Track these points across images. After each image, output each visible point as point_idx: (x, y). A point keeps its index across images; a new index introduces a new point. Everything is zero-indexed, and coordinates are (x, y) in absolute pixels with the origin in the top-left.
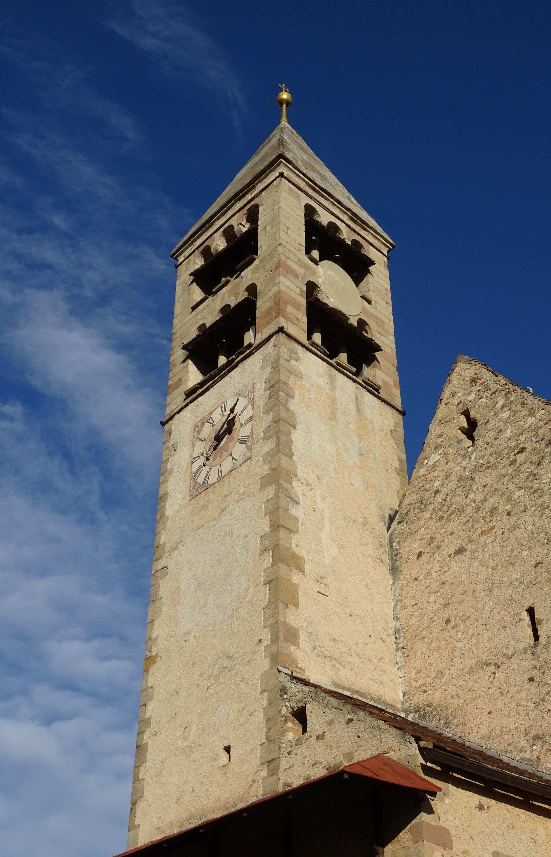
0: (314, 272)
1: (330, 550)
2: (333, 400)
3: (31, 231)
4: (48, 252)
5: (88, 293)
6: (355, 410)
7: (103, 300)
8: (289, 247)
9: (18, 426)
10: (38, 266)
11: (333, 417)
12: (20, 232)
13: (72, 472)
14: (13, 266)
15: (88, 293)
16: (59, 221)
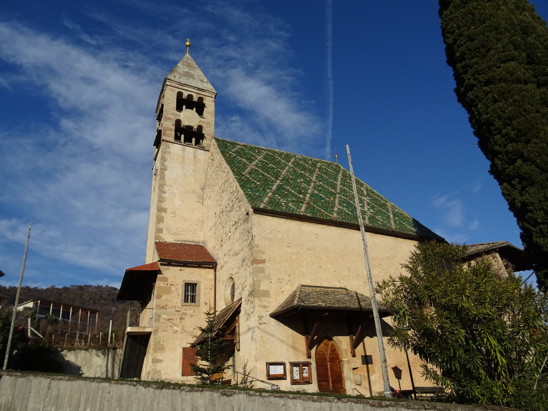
0: (179, 115)
1: (177, 203)
2: (184, 157)
3: (222, 45)
4: (231, 52)
5: (250, 65)
6: (193, 157)
7: (257, 66)
8: (169, 110)
9: (239, 124)
10: (228, 59)
11: (183, 162)
12: (218, 47)
13: (263, 136)
14: (220, 62)
15: (250, 65)
16: (232, 38)
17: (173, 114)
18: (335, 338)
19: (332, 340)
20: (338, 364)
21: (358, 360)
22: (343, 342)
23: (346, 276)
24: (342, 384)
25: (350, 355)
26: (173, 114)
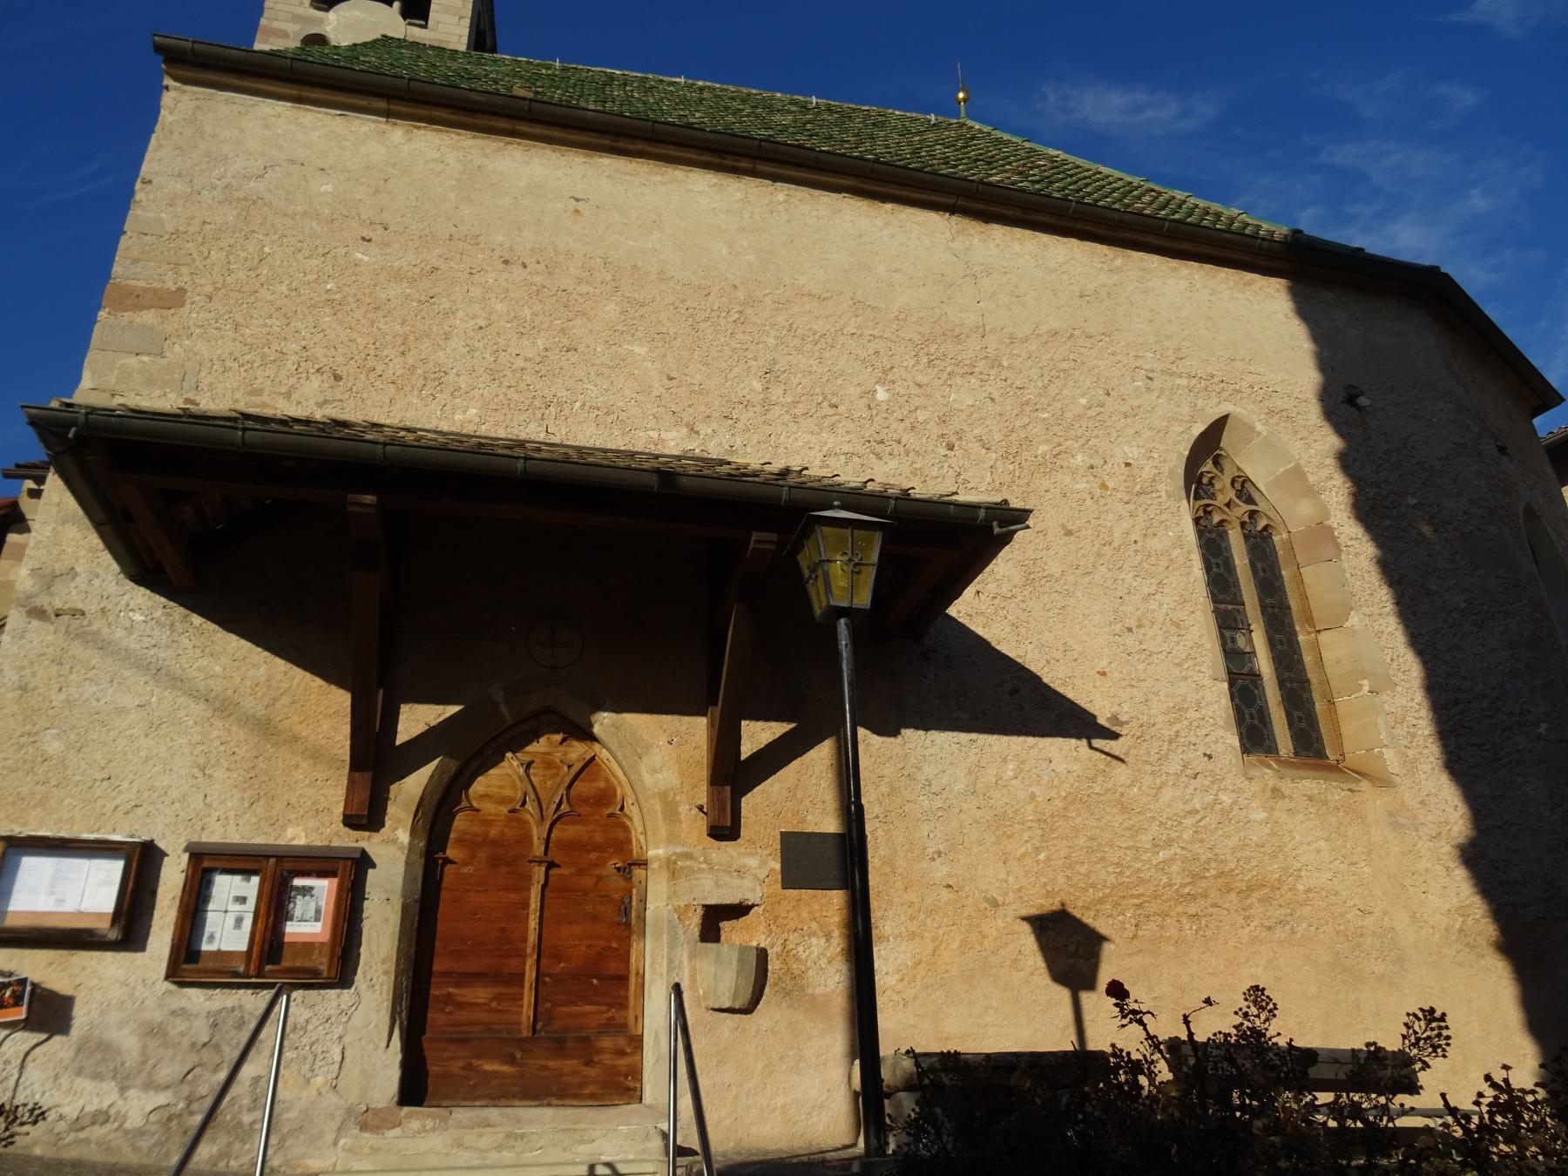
0: (321, 21)
17: (296, 18)
18: (603, 722)
19: (588, 736)
20: (617, 882)
21: (752, 862)
22: (654, 756)
23: (747, 405)
24: (622, 1005)
25: (694, 826)
26: (296, 18)
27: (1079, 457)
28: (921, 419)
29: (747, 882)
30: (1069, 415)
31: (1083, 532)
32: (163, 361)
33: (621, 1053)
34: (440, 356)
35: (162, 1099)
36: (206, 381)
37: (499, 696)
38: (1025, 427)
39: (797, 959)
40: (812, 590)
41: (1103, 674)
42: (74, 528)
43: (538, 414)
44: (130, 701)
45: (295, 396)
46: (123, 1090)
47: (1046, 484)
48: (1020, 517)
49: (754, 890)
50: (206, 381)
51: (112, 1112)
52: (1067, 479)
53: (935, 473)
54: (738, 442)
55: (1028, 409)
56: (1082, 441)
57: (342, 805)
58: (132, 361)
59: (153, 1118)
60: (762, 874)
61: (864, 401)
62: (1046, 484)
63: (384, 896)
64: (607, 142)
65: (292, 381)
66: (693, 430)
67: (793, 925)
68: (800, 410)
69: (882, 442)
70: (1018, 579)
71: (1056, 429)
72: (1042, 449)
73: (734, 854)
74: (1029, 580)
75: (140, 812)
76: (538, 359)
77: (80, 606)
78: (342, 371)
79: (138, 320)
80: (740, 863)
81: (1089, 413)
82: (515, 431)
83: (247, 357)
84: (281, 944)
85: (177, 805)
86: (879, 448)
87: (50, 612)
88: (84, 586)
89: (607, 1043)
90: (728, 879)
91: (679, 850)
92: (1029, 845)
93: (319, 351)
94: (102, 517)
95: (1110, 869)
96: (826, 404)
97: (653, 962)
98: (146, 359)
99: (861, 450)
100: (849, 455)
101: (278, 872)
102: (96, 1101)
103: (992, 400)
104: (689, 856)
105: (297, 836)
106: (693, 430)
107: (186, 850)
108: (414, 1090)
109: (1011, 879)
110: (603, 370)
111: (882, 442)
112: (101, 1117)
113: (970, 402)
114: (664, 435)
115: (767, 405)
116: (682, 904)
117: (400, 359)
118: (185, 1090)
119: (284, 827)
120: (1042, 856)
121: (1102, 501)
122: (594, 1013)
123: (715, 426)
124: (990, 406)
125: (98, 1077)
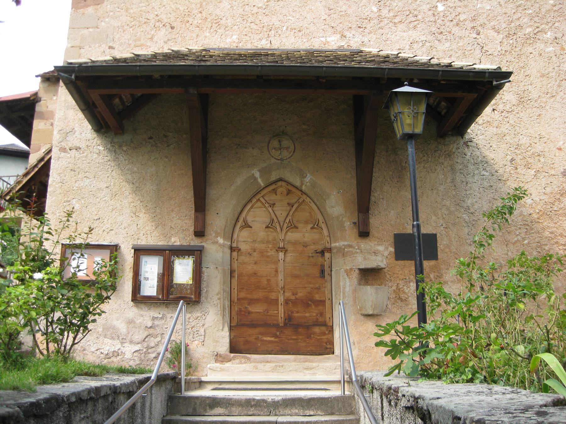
21: (381, 248)
27: (549, 33)
28: (461, 19)
29: (379, 258)
30: (543, 10)
31: (551, 75)
32: (98, 30)
33: (324, 334)
34: (218, 12)
35: (137, 347)
36: (117, 37)
37: (257, 175)
38: (518, 19)
39: (404, 292)
40: (395, 125)
41: (560, 149)
42: (72, 111)
43: (266, 34)
44: (103, 185)
45: (155, 39)
46: (122, 343)
47: (530, 49)
48: (508, 75)
49: (382, 261)
50: (117, 37)
51: (120, 351)
52: (542, 46)
53: (469, 48)
54: (366, 39)
55: (520, 9)
56: (550, 25)
57: (193, 227)
58: (85, 32)
59: (135, 354)
60: (386, 254)
61: (430, 13)
62: (530, 49)
63: (215, 266)
64: (273, 317)
65: (153, 32)
66: (343, 36)
67: (401, 277)
68: (397, 20)
69: (441, 33)
70: (514, 102)
71: (536, 19)
72: (529, 30)
73: (372, 245)
74: (521, 101)
75: (113, 232)
76: (264, 7)
77: (78, 145)
78: (174, 24)
79: (86, 12)
80: (375, 249)
81: (555, 8)
82: (256, 44)
83: (133, 23)
84: (172, 286)
85: (127, 229)
86: (440, 37)
87: (68, 148)
88: (79, 136)
89: (317, 330)
90: (369, 256)
91: (346, 243)
92: (519, 237)
93: (163, 17)
94: (83, 107)
95: (561, 247)
96: (411, 15)
97: (336, 295)
98: (91, 30)
99: (430, 38)
100: (424, 43)
101: (168, 255)
102: (113, 347)
103: (501, 5)
104: (350, 246)
105: (176, 241)
106: (343, 36)
107: (132, 248)
108: (234, 348)
109: (510, 254)
110: (295, 9)
111: (441, 33)
112: (116, 354)
113: (488, 8)
114: (328, 39)
115: (380, 18)
116: (348, 268)
117: (200, 15)
118: (145, 344)
119: (170, 238)
120: (526, 242)
121: (561, 57)
122: (311, 314)
123: (353, 32)
124: (499, 9)
125: (112, 338)
